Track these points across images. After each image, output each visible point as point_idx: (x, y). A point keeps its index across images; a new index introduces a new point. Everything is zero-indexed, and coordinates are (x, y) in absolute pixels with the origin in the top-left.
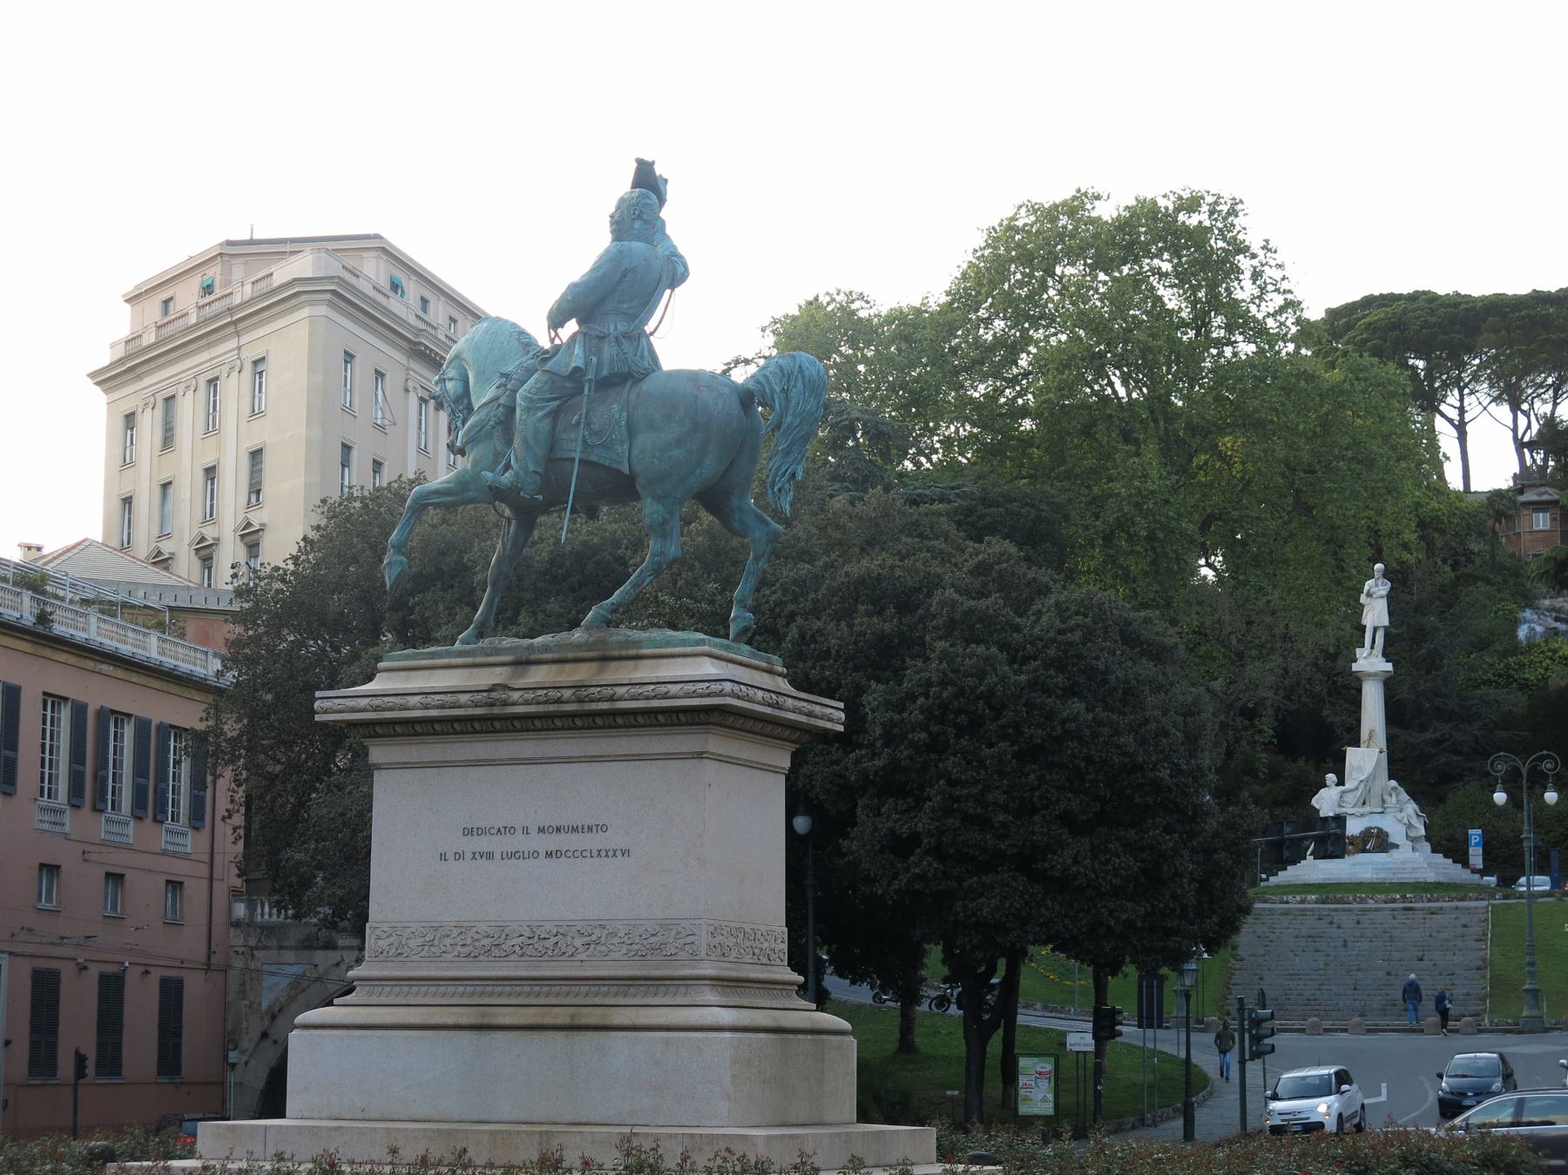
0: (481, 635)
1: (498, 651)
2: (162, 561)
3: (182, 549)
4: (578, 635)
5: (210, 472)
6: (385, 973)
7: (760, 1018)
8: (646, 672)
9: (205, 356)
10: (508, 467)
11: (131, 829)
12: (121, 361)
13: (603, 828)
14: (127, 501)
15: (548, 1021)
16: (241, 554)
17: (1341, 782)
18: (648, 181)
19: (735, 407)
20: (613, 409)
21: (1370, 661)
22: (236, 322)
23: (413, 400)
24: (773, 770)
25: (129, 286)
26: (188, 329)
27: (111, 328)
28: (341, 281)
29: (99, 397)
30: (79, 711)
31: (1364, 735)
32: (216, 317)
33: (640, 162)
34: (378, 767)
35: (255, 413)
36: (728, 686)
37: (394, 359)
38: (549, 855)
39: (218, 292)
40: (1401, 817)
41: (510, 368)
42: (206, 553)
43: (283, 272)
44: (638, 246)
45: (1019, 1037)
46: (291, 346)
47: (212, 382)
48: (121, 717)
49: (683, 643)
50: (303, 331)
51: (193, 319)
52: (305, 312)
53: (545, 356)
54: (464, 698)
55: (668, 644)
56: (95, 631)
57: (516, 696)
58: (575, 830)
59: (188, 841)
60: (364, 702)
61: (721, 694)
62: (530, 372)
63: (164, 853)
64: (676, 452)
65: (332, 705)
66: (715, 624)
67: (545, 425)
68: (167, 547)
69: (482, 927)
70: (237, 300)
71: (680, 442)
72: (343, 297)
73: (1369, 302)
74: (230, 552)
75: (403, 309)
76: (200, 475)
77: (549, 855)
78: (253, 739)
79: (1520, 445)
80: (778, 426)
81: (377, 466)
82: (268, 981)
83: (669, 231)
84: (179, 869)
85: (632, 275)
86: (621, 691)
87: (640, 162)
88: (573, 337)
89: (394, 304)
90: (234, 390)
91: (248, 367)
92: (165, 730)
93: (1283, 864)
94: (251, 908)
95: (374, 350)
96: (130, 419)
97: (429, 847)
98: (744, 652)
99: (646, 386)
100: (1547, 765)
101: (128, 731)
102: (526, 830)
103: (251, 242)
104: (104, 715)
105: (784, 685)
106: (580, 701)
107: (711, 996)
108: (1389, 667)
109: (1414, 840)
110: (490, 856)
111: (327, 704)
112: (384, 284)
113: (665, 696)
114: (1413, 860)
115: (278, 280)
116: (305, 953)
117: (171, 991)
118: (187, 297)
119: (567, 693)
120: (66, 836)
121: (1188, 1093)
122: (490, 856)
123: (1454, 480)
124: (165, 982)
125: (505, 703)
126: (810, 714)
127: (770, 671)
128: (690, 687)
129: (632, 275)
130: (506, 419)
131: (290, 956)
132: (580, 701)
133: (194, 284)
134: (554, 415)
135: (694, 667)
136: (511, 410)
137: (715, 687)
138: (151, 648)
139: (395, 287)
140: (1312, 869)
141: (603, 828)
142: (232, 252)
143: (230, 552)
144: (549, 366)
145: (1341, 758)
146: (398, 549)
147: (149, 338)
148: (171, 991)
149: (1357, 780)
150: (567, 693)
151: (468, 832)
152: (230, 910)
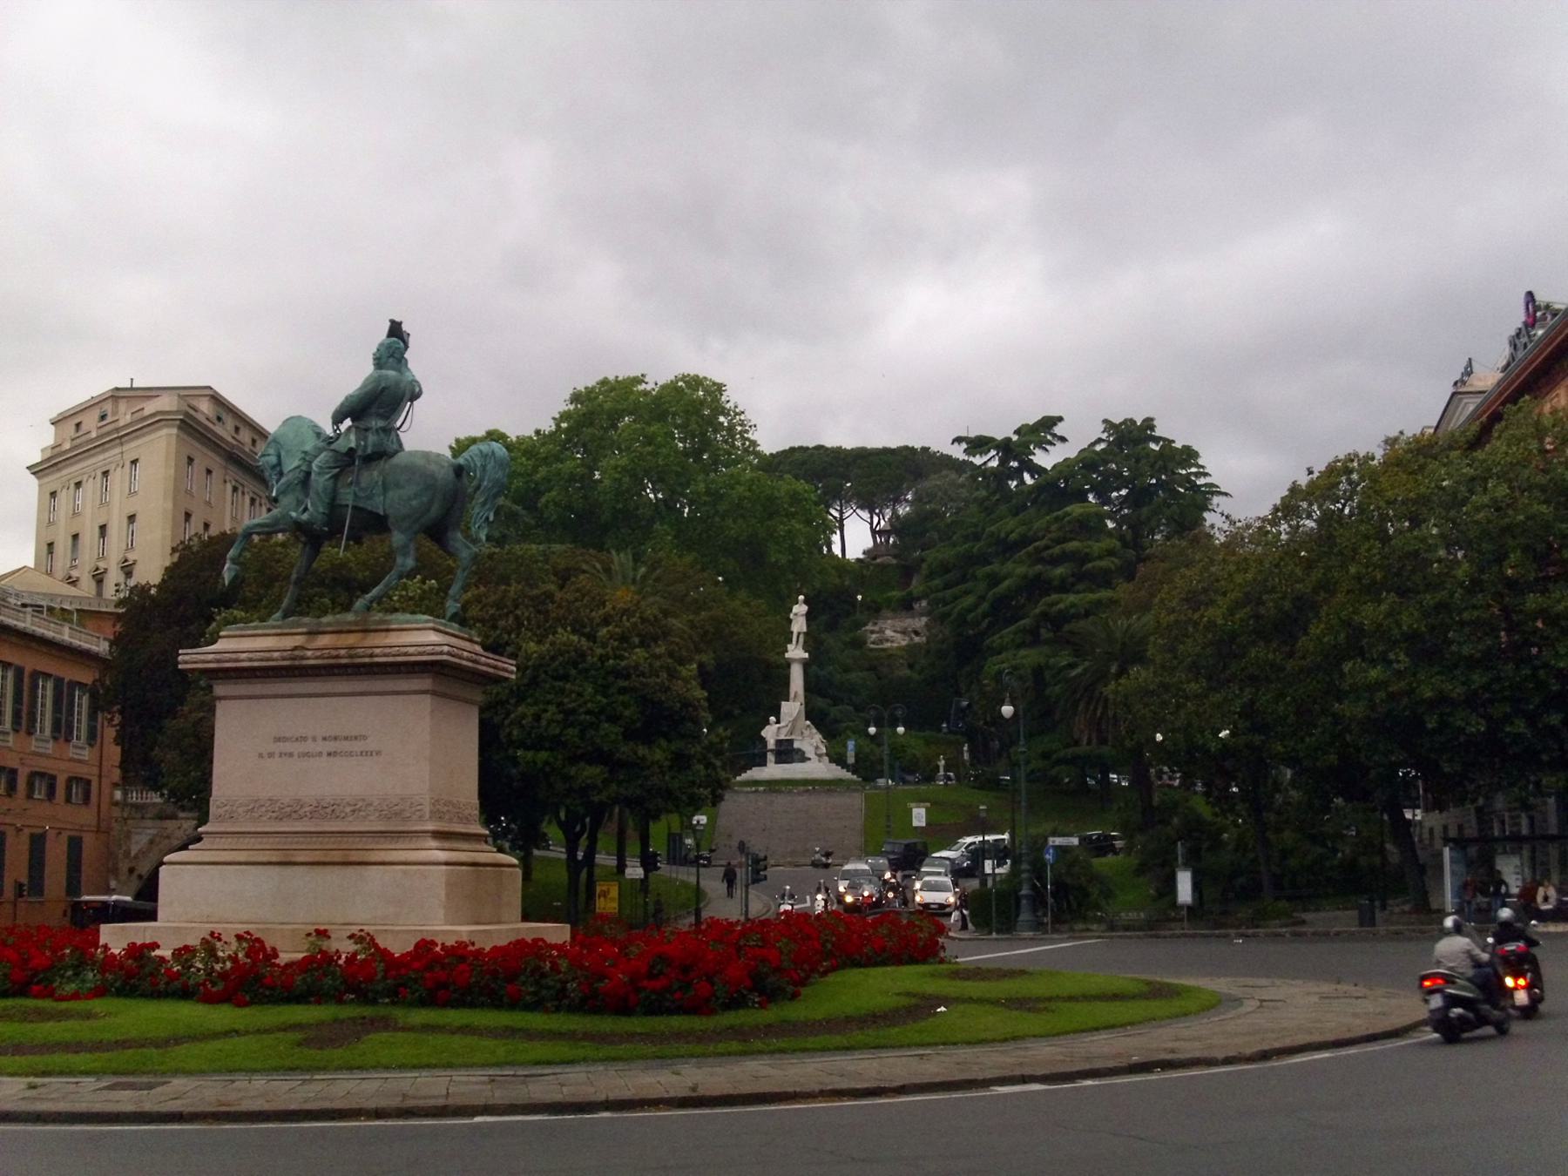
0: (285, 616)
1: (299, 626)
2: (73, 582)
3: (84, 575)
4: (350, 617)
5: (103, 528)
6: (222, 829)
7: (463, 857)
8: (394, 639)
9: (101, 457)
10: (306, 509)
11: (51, 745)
12: (49, 459)
13: (364, 738)
14: (51, 545)
15: (328, 859)
16: (121, 578)
17: (778, 722)
18: (396, 330)
19: (452, 475)
20: (372, 475)
21: (796, 652)
22: (121, 437)
23: (229, 487)
24: (471, 702)
25: (54, 414)
26: (88, 441)
27: (38, 441)
28: (187, 414)
29: (33, 481)
30: (19, 672)
31: (792, 695)
32: (108, 433)
33: (393, 322)
34: (220, 698)
35: (132, 493)
36: (446, 649)
37: (216, 462)
38: (329, 754)
39: (109, 419)
40: (810, 741)
41: (308, 447)
42: (99, 577)
43: (150, 407)
44: (392, 373)
45: (597, 871)
46: (158, 453)
47: (106, 474)
48: (47, 676)
49: (417, 622)
50: (163, 444)
51: (94, 435)
52: (165, 431)
53: (330, 441)
54: (276, 655)
55: (408, 622)
56: (27, 623)
57: (309, 653)
58: (346, 738)
59: (86, 752)
60: (211, 657)
61: (441, 653)
62: (321, 450)
63: (71, 760)
64: (414, 503)
65: (189, 658)
66: (436, 611)
67: (330, 483)
68: (75, 574)
69: (286, 801)
70: (122, 423)
71: (416, 496)
72: (189, 426)
73: (792, 449)
74: (114, 576)
75: (225, 431)
76: (97, 530)
77: (329, 754)
78: (140, 680)
79: (874, 532)
80: (478, 487)
81: (206, 526)
82: (135, 838)
83: (410, 365)
84: (82, 771)
85: (381, 402)
86: (377, 651)
87: (393, 322)
88: (349, 429)
89: (218, 429)
90: (118, 478)
91: (128, 464)
92: (74, 685)
93: (745, 769)
94: (125, 794)
95: (206, 458)
96: (53, 494)
97: (254, 750)
98: (454, 628)
99: (399, 459)
100: (899, 712)
101: (50, 685)
102: (314, 739)
103: (132, 389)
104: (35, 675)
105: (478, 648)
106: (351, 657)
107: (434, 844)
108: (806, 655)
109: (820, 756)
110: (291, 755)
111: (187, 658)
112: (212, 415)
113: (406, 654)
114: (817, 767)
115: (147, 412)
116: (158, 823)
117: (75, 845)
118: (91, 422)
119: (343, 652)
120: (10, 749)
121: (698, 902)
122: (291, 755)
123: (837, 550)
124: (71, 839)
125: (303, 658)
126: (495, 667)
127: (471, 641)
128: (421, 649)
129: (381, 402)
130: (305, 480)
131: (149, 823)
132: (351, 657)
133: (96, 413)
134: (336, 477)
135: (422, 637)
136: (308, 474)
137: (438, 649)
138: (65, 635)
139: (219, 419)
140: (772, 770)
141: (364, 738)
142: (116, 395)
143: (114, 576)
144: (333, 447)
145: (779, 707)
146: (233, 561)
147: (67, 446)
148: (75, 845)
149: (790, 718)
150: (343, 652)
151: (278, 740)
152: (112, 795)
